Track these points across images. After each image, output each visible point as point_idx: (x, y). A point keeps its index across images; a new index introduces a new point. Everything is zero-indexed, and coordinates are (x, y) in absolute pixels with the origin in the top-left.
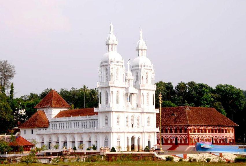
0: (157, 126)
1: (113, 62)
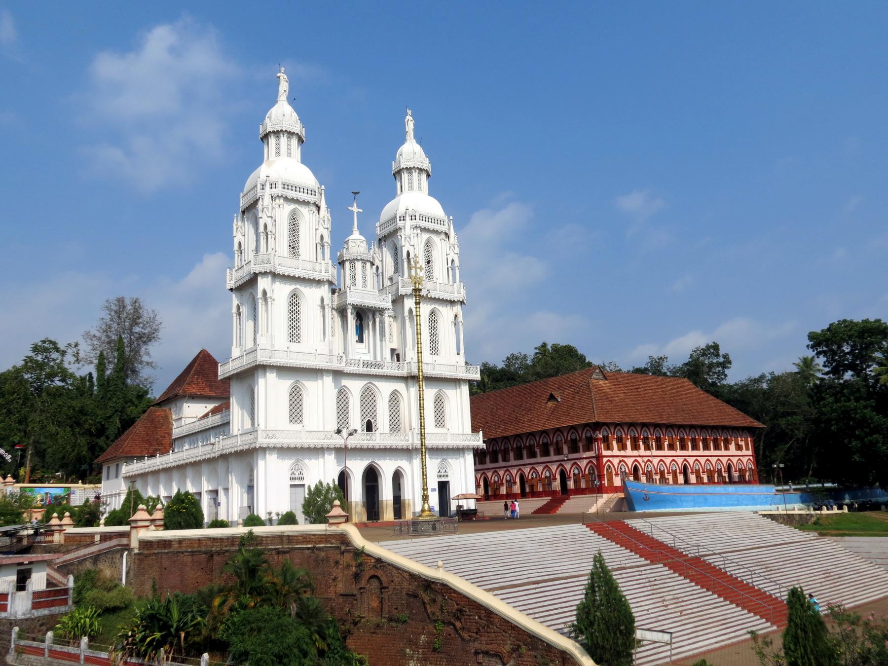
0: (475, 430)
1: (273, 186)
